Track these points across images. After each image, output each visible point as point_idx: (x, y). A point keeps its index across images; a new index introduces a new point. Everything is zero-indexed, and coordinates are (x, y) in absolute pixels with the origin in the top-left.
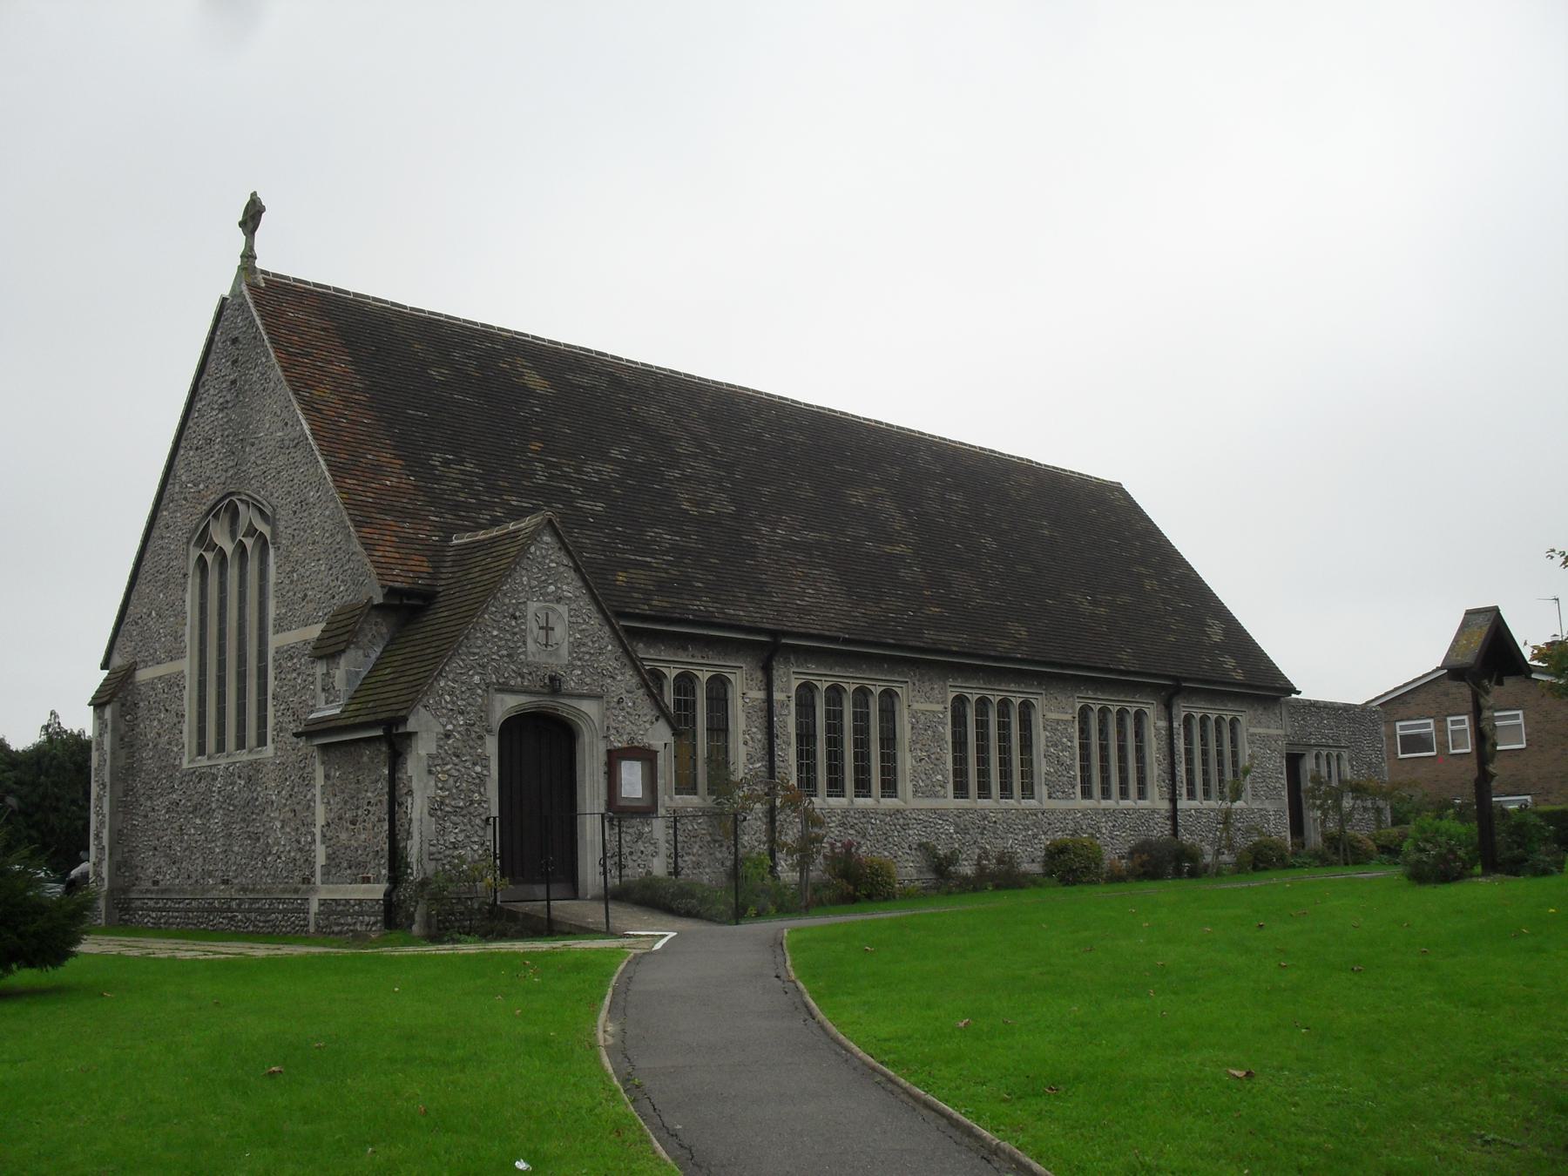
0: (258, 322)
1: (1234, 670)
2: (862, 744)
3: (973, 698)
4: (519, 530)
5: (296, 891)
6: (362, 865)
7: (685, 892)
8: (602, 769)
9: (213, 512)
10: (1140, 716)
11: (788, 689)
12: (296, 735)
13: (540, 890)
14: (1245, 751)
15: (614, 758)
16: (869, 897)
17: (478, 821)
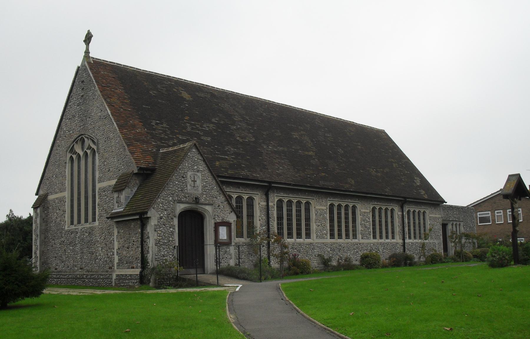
0: (91, 75)
1: (424, 195)
2: (299, 221)
3: (336, 204)
4: (184, 147)
5: (107, 271)
6: (131, 263)
7: (243, 271)
8: (213, 229)
9: (76, 141)
10: (392, 211)
11: (274, 202)
12: (108, 218)
13: (193, 271)
14: (428, 222)
15: (217, 225)
16: (302, 273)
17: (171, 247)
